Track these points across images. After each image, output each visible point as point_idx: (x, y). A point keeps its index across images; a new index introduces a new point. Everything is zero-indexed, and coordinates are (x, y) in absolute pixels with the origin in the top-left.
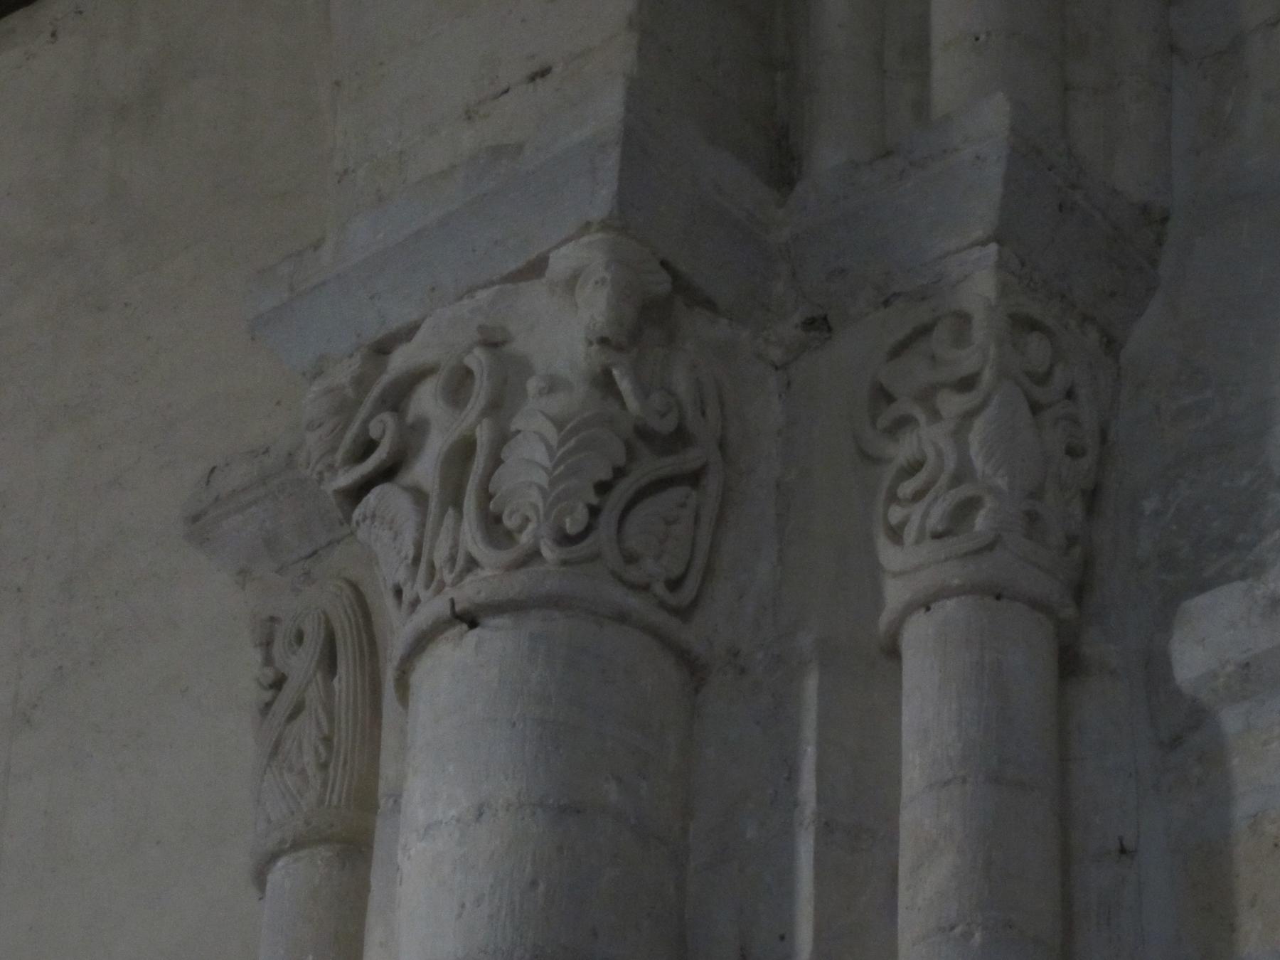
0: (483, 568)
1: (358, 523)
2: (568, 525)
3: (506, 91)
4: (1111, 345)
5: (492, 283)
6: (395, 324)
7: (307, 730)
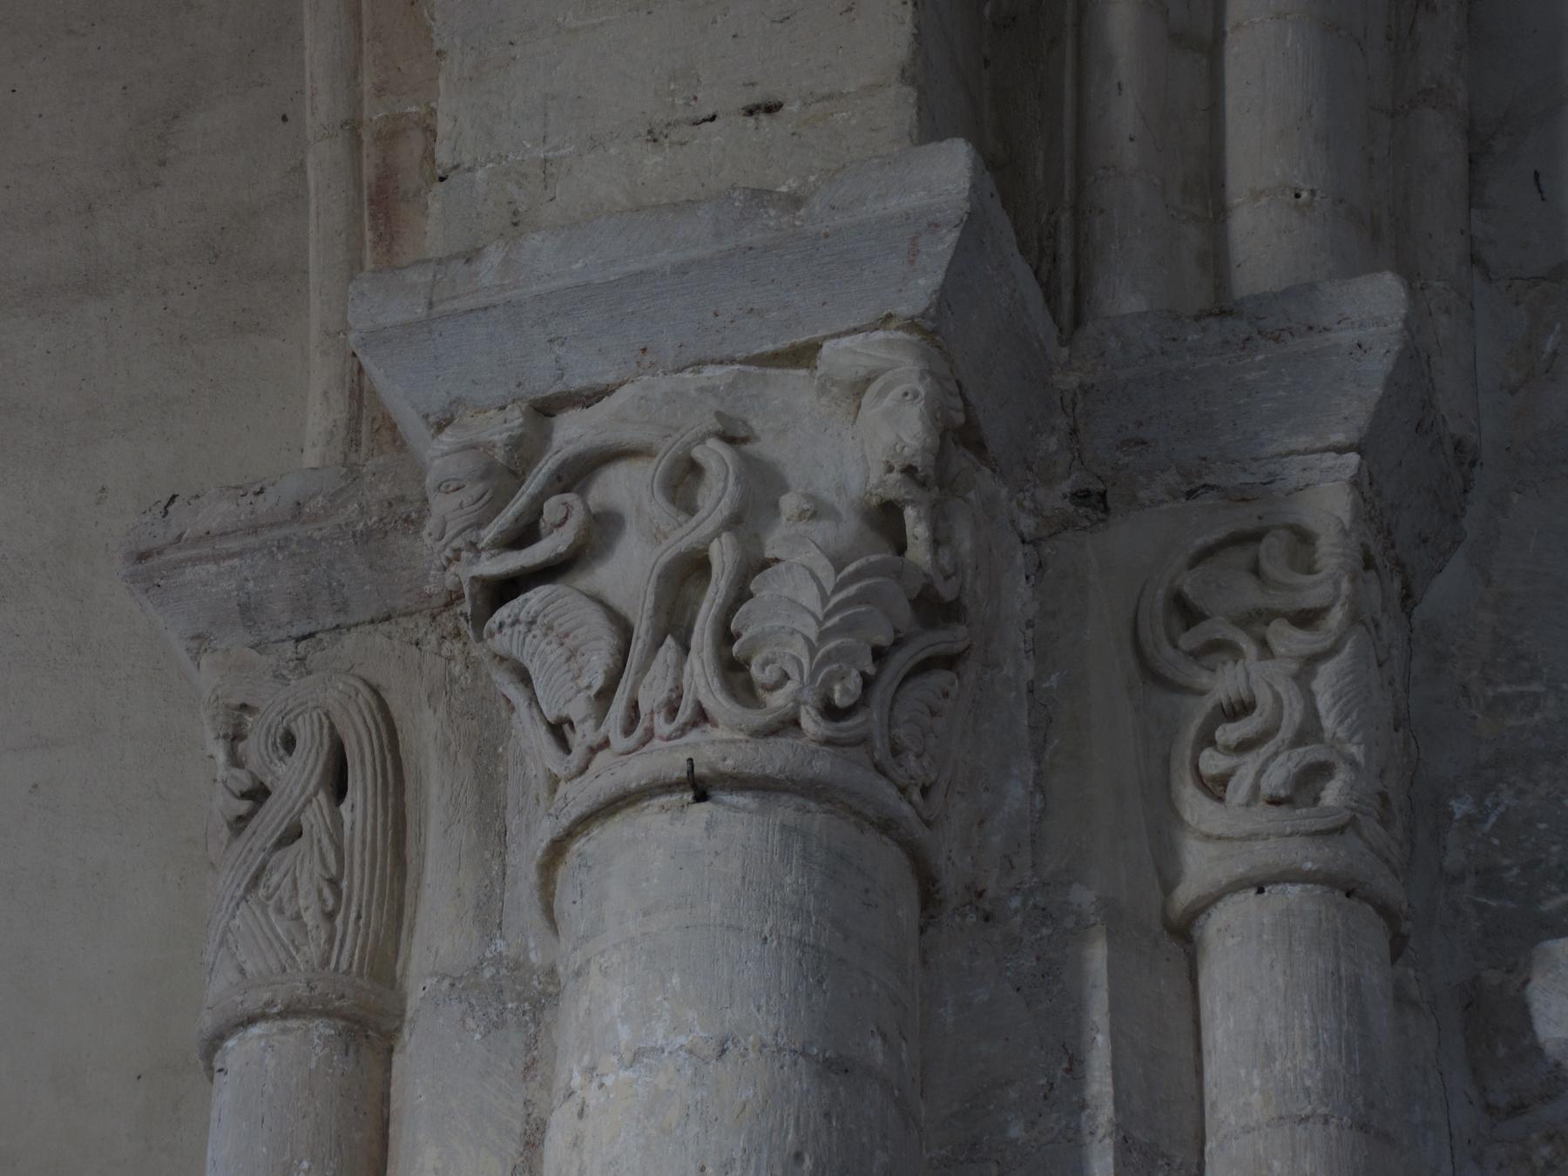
0: (715, 725)
1: (501, 625)
2: (837, 696)
3: (713, 118)
4: (1408, 598)
5: (733, 361)
6: (577, 382)
7: (304, 867)
